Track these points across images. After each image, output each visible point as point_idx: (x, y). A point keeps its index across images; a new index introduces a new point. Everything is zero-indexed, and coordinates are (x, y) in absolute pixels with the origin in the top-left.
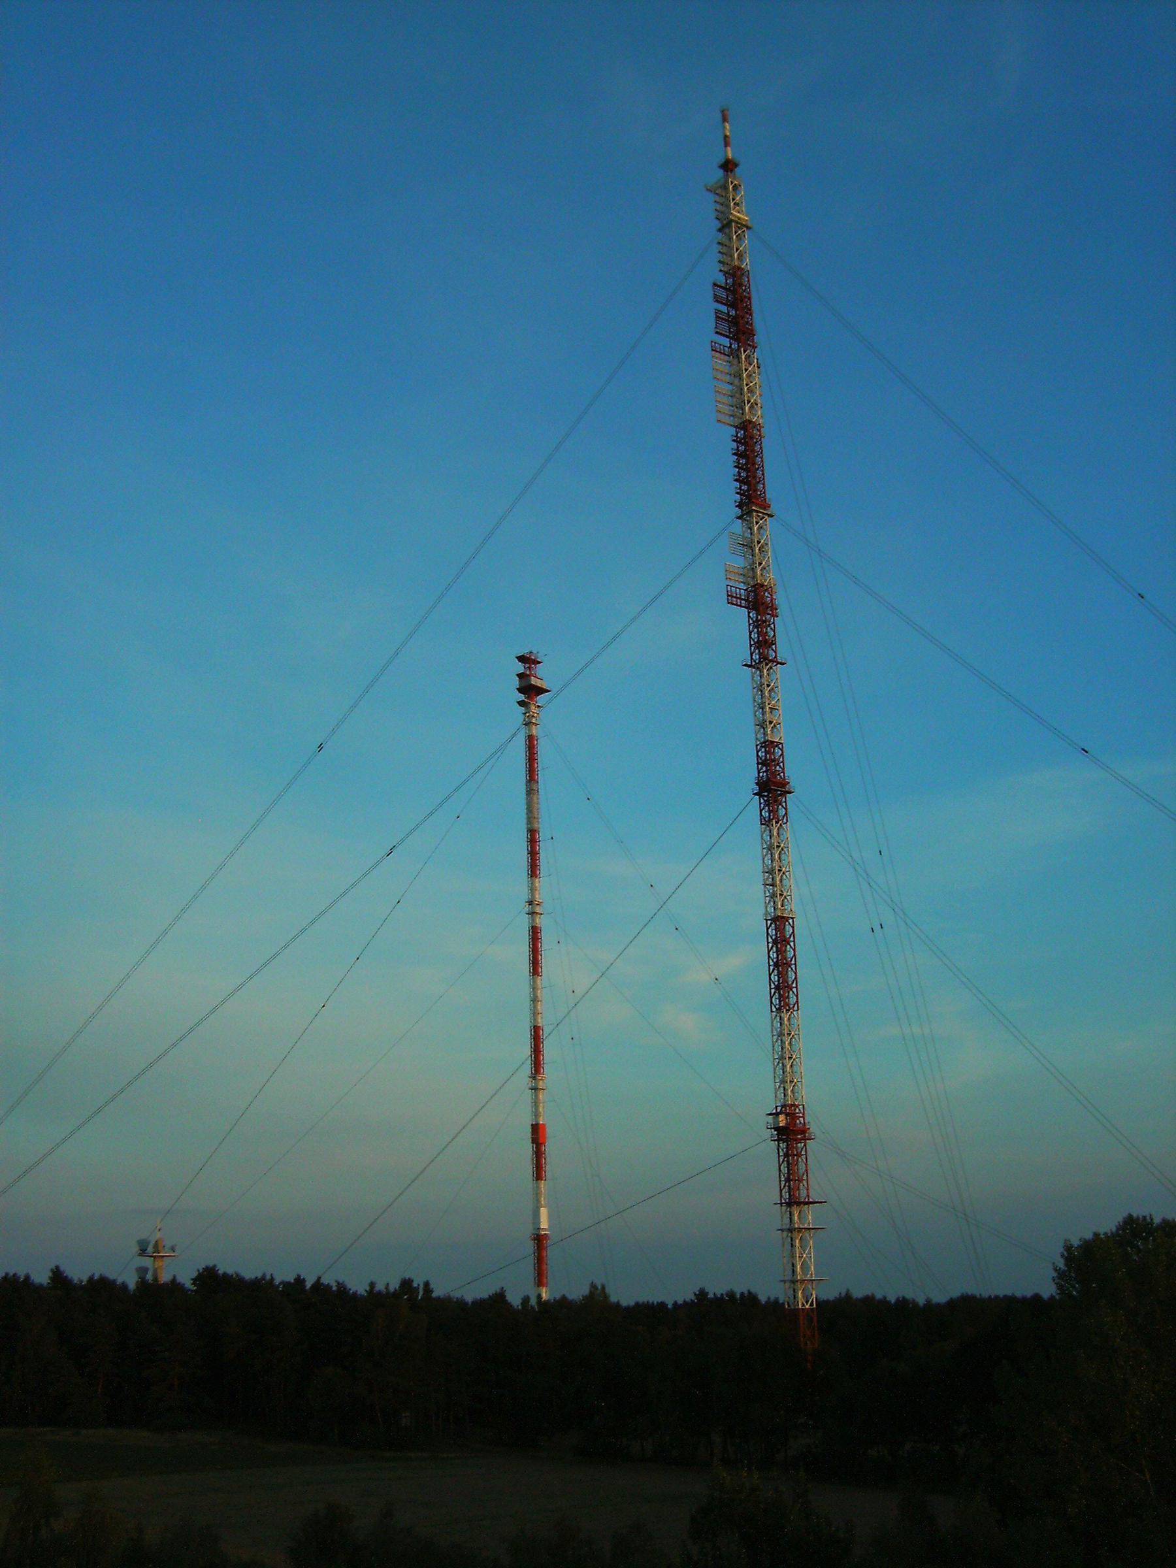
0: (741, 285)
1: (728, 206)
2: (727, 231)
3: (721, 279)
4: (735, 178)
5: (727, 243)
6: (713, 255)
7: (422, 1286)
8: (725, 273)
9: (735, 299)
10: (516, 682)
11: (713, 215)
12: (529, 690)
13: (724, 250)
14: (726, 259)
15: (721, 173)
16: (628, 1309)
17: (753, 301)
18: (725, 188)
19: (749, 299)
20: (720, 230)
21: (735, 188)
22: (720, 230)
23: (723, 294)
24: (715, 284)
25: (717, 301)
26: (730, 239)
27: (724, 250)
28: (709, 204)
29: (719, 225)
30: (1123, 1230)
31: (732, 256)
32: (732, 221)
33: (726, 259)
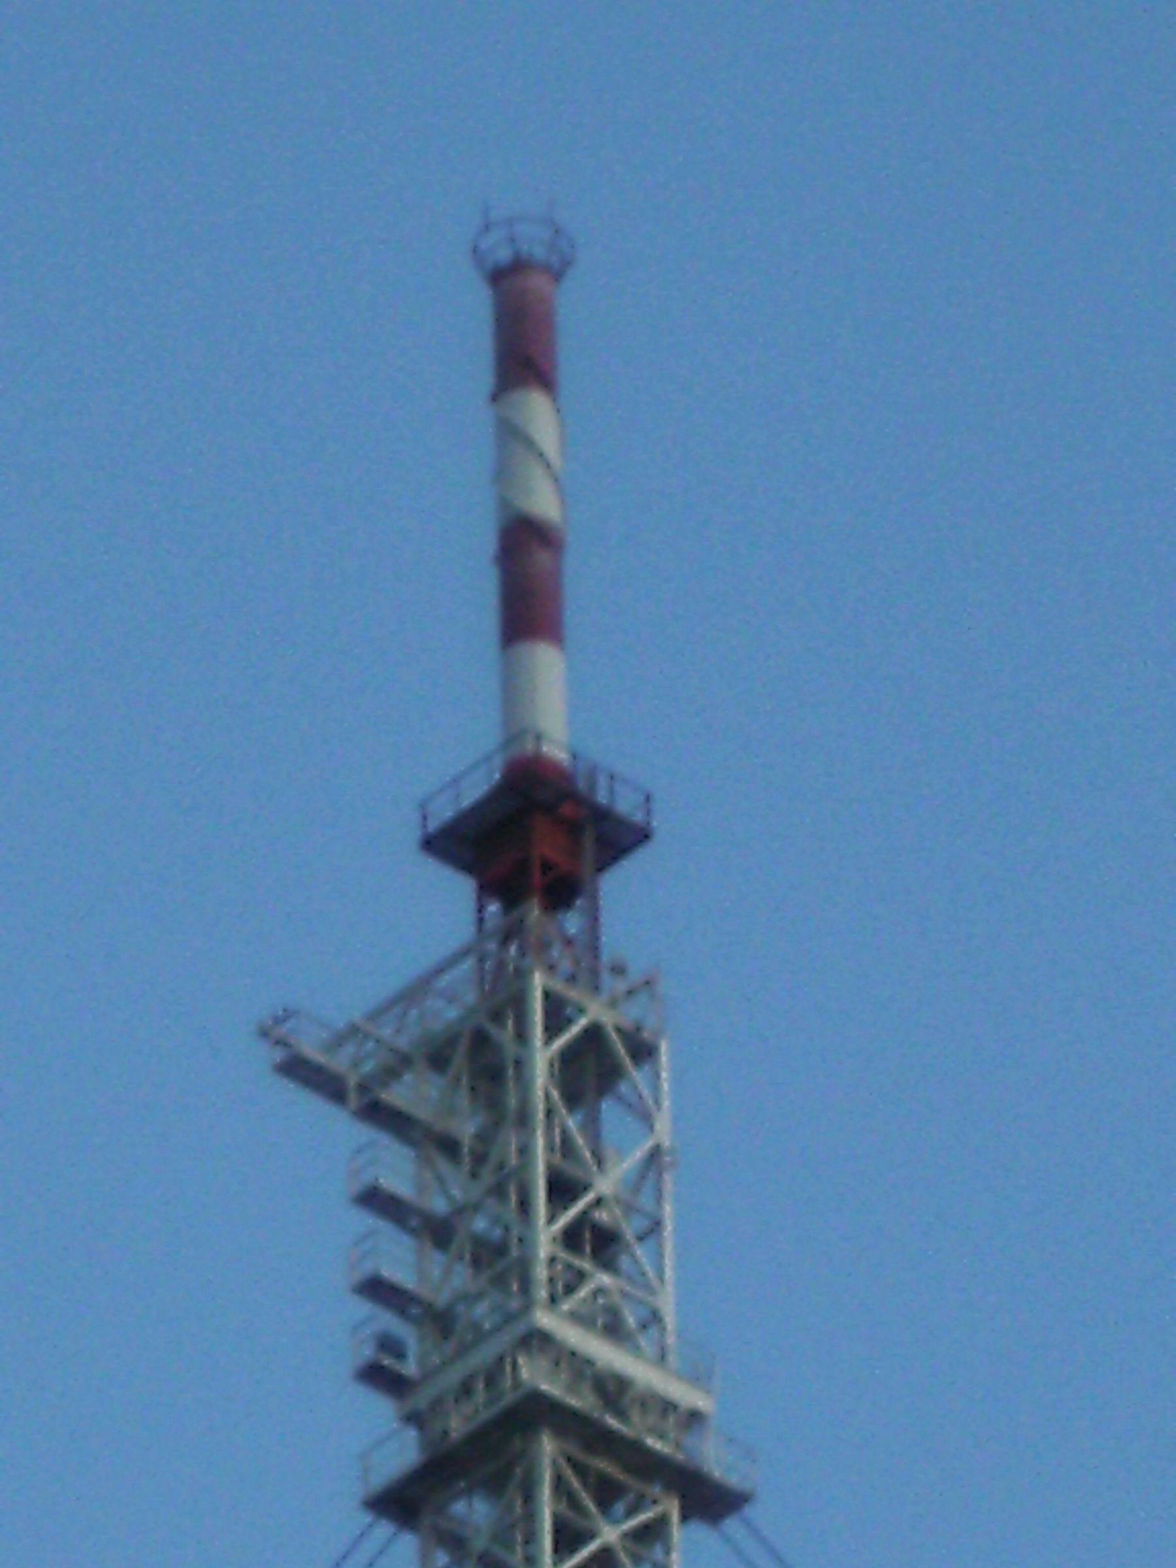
1: (498, 1260)
11: (347, 1328)
15: (448, 904)
18: (479, 1058)
20: (400, 1503)
21: (592, 1069)
22: (400, 1503)
28: (296, 1219)
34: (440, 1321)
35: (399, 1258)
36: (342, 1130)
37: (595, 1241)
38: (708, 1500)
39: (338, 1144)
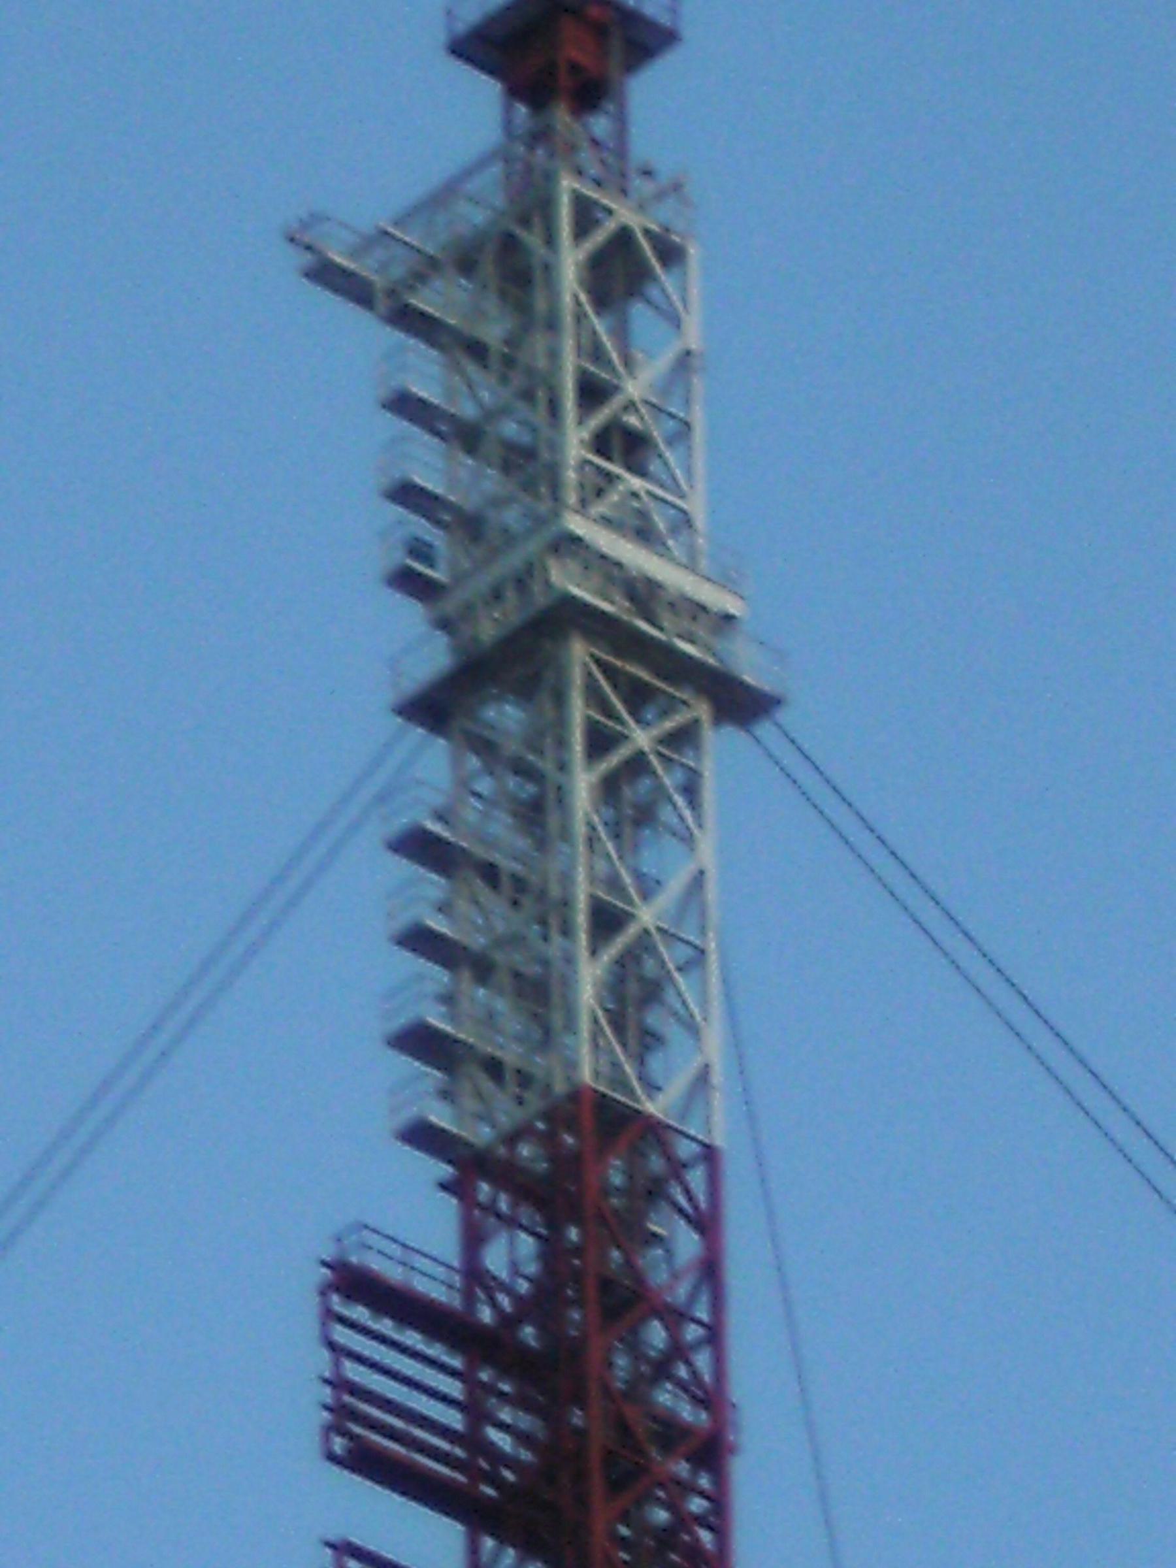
0: (626, 1302)
1: (527, 464)
2: (506, 716)
3: (418, 1226)
4: (617, 177)
5: (498, 836)
6: (349, 965)
7: (626, 731)
8: (469, 1168)
9: (559, 1455)
11: (377, 533)
13: (474, 921)
14: (487, 1018)
15: (477, 107)
16: (544, 1420)
17: (743, 1471)
18: (507, 262)
19: (711, 1452)
20: (431, 709)
21: (621, 272)
22: (431, 709)
23: (426, 1386)
24: (352, 1282)
25: (365, 1462)
26: (537, 813)
27: (474, 921)
28: (332, 413)
29: (432, 658)
30: (549, 1140)
31: (539, 994)
32: (566, 616)
33: (487, 1018)
34: (470, 526)
35: (430, 464)
36: (365, 337)
37: (624, 445)
38: (740, 704)
39: (365, 348)
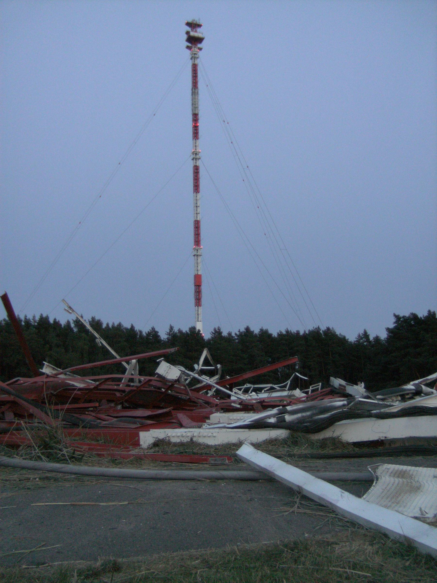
10: (185, 37)
12: (194, 41)
